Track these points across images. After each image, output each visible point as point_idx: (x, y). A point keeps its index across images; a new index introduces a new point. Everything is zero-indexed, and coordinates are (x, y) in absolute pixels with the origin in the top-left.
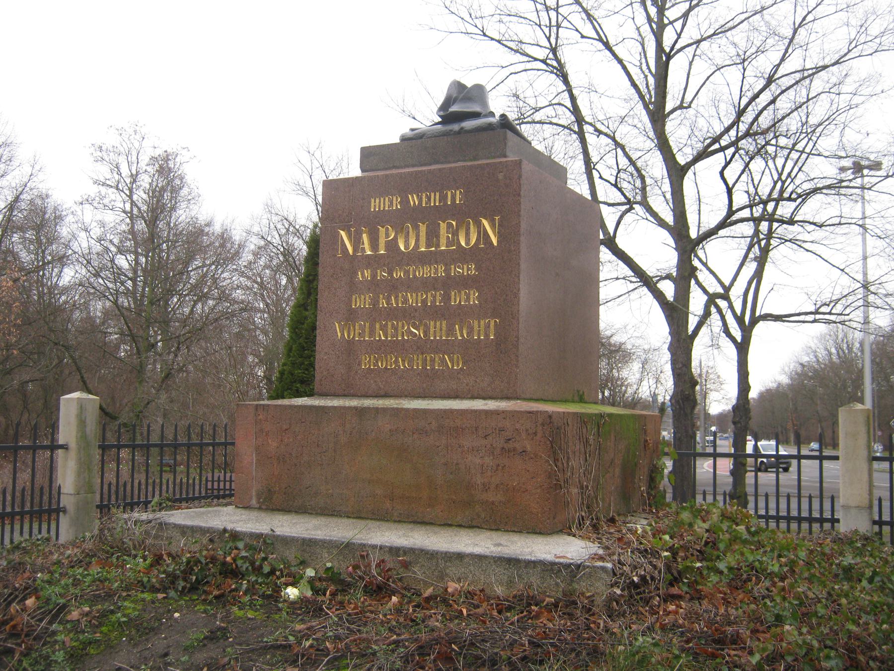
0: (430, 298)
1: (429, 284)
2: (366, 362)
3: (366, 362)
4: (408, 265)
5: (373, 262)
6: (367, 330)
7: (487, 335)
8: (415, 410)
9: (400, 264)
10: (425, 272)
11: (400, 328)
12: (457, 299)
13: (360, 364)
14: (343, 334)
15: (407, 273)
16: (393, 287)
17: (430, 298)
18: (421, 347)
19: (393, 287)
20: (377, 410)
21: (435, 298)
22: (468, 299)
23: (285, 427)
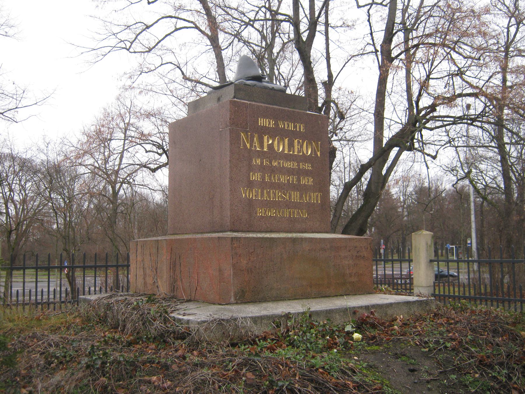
0: (291, 179)
1: (290, 172)
2: (260, 212)
3: (260, 212)
4: (279, 159)
5: (261, 154)
6: (260, 194)
7: (317, 201)
8: (320, 239)
9: (275, 158)
10: (289, 165)
11: (277, 194)
12: (304, 181)
13: (256, 213)
14: (246, 195)
15: (279, 163)
16: (273, 171)
17: (291, 179)
18: (288, 205)
19: (273, 171)
20: (302, 239)
21: (293, 179)
22: (308, 181)
23: (251, 251)
